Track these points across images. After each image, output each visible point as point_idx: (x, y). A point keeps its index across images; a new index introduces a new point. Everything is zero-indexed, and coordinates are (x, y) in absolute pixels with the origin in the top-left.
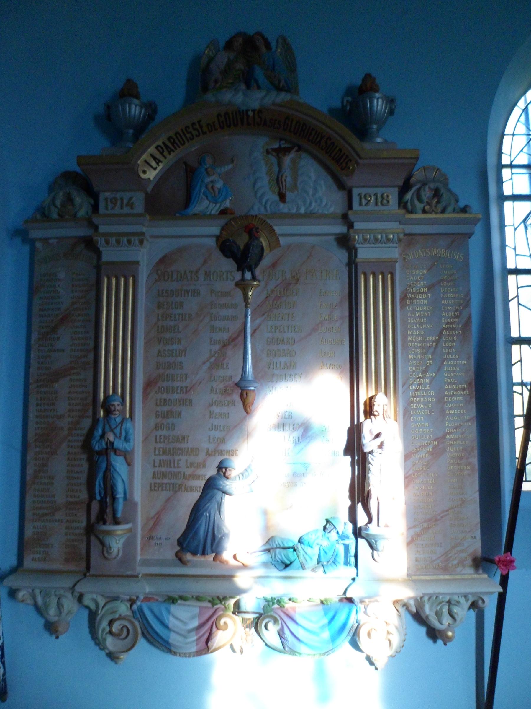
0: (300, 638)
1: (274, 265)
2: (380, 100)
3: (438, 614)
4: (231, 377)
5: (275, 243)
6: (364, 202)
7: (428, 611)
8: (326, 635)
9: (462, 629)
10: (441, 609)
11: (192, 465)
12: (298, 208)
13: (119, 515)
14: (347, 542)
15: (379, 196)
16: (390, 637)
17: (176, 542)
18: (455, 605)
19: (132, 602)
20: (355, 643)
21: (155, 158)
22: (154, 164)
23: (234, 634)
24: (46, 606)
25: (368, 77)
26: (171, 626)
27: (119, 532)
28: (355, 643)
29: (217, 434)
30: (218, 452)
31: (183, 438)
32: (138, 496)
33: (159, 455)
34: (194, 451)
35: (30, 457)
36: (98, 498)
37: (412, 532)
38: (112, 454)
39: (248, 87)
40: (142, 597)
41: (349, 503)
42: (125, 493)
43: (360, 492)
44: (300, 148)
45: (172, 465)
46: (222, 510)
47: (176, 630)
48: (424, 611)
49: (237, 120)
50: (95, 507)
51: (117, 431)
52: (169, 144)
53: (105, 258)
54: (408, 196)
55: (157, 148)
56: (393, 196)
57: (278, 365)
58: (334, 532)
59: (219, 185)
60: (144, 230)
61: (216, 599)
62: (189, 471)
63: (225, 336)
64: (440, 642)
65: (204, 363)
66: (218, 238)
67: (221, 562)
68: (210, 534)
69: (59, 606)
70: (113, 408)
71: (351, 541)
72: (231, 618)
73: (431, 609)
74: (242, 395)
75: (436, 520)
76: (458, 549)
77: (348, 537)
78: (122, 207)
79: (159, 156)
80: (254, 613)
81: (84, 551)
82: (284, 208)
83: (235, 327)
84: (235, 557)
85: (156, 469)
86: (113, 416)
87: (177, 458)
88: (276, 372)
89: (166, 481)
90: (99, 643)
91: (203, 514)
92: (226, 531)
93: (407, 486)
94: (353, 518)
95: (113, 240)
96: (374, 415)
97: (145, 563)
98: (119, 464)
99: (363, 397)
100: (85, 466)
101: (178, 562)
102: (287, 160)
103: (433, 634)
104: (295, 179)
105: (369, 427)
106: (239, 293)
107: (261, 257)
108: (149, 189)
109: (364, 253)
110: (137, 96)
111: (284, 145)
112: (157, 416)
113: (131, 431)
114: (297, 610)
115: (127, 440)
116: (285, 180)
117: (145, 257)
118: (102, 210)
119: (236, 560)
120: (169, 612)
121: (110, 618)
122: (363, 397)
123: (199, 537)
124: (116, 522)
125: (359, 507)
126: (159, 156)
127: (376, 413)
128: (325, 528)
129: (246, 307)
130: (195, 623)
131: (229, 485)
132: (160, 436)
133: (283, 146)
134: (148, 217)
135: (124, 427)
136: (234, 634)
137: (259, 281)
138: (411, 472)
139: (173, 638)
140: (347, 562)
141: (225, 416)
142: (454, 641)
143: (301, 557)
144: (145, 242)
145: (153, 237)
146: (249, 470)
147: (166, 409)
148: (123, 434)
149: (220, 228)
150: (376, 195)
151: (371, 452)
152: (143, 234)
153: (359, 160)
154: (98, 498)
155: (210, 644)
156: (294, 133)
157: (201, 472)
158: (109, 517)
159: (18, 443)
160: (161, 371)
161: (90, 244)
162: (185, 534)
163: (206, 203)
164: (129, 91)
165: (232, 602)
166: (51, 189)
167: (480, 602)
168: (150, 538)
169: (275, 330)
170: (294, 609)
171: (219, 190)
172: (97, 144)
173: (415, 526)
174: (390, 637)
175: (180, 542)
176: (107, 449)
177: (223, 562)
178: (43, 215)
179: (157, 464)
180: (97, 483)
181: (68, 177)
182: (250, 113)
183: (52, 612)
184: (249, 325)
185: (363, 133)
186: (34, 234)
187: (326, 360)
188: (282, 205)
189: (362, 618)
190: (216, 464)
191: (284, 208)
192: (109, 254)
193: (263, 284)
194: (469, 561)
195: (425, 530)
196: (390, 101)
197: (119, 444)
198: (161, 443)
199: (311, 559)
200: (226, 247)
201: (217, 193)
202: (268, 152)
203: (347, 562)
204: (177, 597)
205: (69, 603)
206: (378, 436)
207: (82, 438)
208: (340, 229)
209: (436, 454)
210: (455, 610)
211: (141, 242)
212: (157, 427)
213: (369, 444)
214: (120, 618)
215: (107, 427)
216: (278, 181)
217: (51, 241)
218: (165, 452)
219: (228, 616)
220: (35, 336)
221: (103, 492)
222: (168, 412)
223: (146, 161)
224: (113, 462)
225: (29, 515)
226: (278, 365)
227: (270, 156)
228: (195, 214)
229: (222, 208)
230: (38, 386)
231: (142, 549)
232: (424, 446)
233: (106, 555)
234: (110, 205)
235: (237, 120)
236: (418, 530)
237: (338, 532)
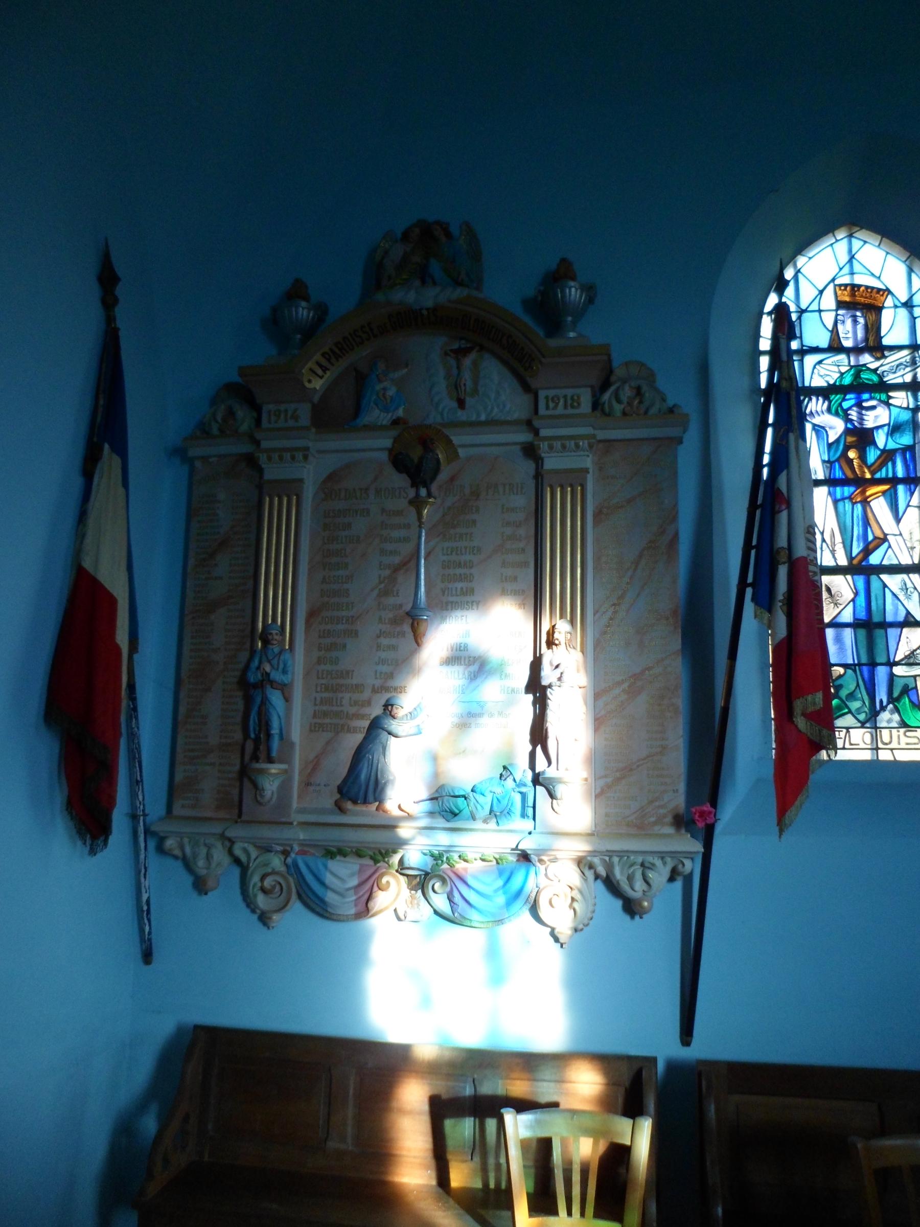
0: (471, 902)
1: (452, 479)
2: (573, 290)
3: (630, 879)
4: (401, 606)
5: (453, 455)
6: (551, 405)
7: (619, 875)
8: (501, 899)
9: (665, 903)
10: (633, 873)
11: (356, 703)
12: (478, 415)
13: (274, 754)
14: (523, 789)
15: (569, 398)
16: (576, 905)
17: (336, 790)
18: (649, 868)
19: (286, 853)
20: (534, 910)
21: (321, 366)
22: (320, 372)
23: (398, 895)
24: (195, 856)
25: (564, 261)
26: (327, 882)
27: (273, 771)
28: (534, 910)
29: (385, 668)
30: (385, 689)
31: (348, 672)
32: (296, 734)
33: (321, 691)
34: (359, 688)
35: (182, 695)
36: (253, 736)
37: (601, 783)
38: (268, 687)
39: (424, 282)
40: (296, 848)
41: (530, 748)
42: (281, 730)
43: (539, 735)
44: (482, 348)
45: (334, 703)
46: (387, 753)
47: (333, 887)
48: (614, 876)
49: (409, 320)
50: (249, 746)
51: (275, 662)
52: (337, 350)
53: (268, 476)
54: (606, 396)
55: (323, 355)
56: (586, 398)
57: (454, 592)
58: (510, 780)
59: (392, 392)
60: (310, 444)
61: (376, 850)
62: (353, 710)
63: (397, 560)
64: (637, 917)
65: (372, 590)
66: (390, 451)
67: (384, 811)
68: (373, 778)
69: (209, 857)
70: (270, 637)
71: (529, 789)
72: (394, 876)
73: (622, 873)
74: (413, 625)
75: (631, 770)
76: (657, 804)
77: (525, 785)
78: (286, 421)
79: (324, 362)
80: (419, 869)
81: (236, 798)
82: (462, 415)
83: (406, 549)
84: (399, 807)
85: (317, 708)
86: (271, 647)
87: (340, 695)
88: (451, 599)
89: (328, 720)
90: (250, 904)
91: (365, 756)
92: (391, 778)
93: (596, 729)
94: (532, 765)
95: (276, 456)
96: (556, 645)
97: (302, 811)
98: (276, 698)
99: (546, 626)
100: (241, 705)
101: (338, 811)
102: (467, 362)
103: (631, 908)
104: (476, 382)
105: (548, 656)
106: (413, 510)
107: (437, 470)
108: (316, 399)
109: (551, 463)
110: (306, 298)
111: (464, 344)
112: (320, 649)
113: (290, 663)
114: (469, 871)
115: (285, 672)
116: (465, 385)
117: (310, 475)
118: (265, 423)
119: (402, 810)
120: (326, 867)
121: (264, 872)
122: (546, 626)
123: (361, 784)
124: (270, 760)
125: (539, 749)
126: (324, 362)
127: (557, 642)
128: (501, 775)
129: (420, 527)
130: (354, 882)
131: (394, 726)
132: (323, 671)
133: (463, 346)
134: (314, 430)
135: (282, 658)
136: (398, 895)
137: (435, 498)
138: (603, 713)
139: (330, 897)
140: (524, 815)
141: (394, 648)
142: (652, 913)
143: (472, 804)
144: (311, 458)
145: (320, 452)
146: (418, 709)
147: (328, 641)
148: (281, 666)
149: (392, 441)
150: (565, 397)
151: (550, 686)
152: (307, 449)
153: (543, 360)
154: (253, 736)
155: (371, 904)
156: (475, 332)
157: (366, 710)
158: (262, 756)
159: (171, 684)
160: (326, 599)
161: (251, 461)
162: (345, 781)
163: (377, 412)
164: (298, 291)
165: (395, 859)
166: (214, 401)
167: (680, 866)
168: (308, 784)
169: (452, 552)
170: (465, 870)
171: (392, 397)
172: (263, 351)
173: (606, 776)
174: (576, 905)
175: (340, 790)
176: (262, 681)
177: (385, 811)
178: (203, 431)
179: (318, 702)
180: (252, 717)
181: (231, 389)
182: (425, 312)
183: (201, 863)
184: (423, 547)
185: (554, 326)
186: (193, 452)
187: (507, 587)
188: (460, 413)
189: (543, 881)
190: (383, 702)
191: (462, 415)
192: (272, 472)
193: (439, 501)
194: (669, 819)
195: (618, 780)
196: (590, 291)
197: (276, 676)
198: (323, 678)
199: (483, 808)
200: (399, 461)
201: (389, 401)
202: (446, 354)
203: (524, 815)
204: (335, 850)
205: (219, 854)
206: (557, 667)
207: (238, 674)
208: (524, 437)
209: (633, 692)
210: (650, 875)
211: (306, 457)
212: (319, 661)
213: (548, 675)
214: (274, 872)
215: (264, 658)
216: (456, 386)
217: (211, 460)
218: (327, 688)
219: (391, 874)
220: (191, 562)
221: (257, 729)
222: (331, 644)
223: (311, 370)
224: (269, 696)
225: (180, 757)
226: (454, 592)
227: (449, 358)
228: (364, 426)
229: (394, 418)
230: (193, 618)
231: (299, 797)
232: (619, 683)
233: (259, 798)
234: (273, 418)
235: (409, 320)
236: (609, 780)
237: (514, 780)
